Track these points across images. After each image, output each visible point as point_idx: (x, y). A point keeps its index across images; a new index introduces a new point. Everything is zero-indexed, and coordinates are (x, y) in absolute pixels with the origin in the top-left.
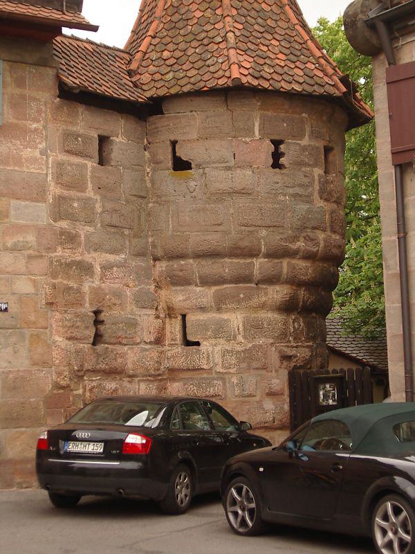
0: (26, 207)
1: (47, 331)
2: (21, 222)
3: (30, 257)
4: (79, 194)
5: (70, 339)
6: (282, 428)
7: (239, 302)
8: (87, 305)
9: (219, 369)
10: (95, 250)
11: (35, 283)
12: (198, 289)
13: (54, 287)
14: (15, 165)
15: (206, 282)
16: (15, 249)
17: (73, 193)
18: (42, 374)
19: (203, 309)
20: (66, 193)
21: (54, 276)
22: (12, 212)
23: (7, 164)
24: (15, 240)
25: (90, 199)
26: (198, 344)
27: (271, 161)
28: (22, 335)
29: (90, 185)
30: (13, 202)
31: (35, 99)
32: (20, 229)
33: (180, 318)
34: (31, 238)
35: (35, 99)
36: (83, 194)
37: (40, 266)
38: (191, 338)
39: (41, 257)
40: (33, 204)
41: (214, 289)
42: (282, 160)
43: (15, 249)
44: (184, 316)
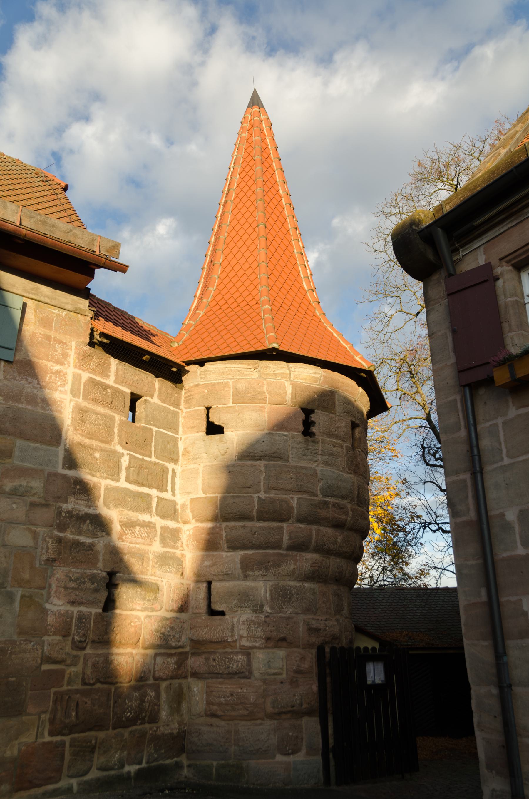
0: (36, 449)
1: (44, 592)
2: (27, 465)
3: (33, 505)
4: (103, 445)
5: (73, 603)
6: (309, 713)
7: (267, 569)
8: (100, 565)
9: (245, 643)
10: (116, 506)
11: (35, 536)
12: (224, 554)
13: (60, 540)
14: (28, 403)
15: (233, 546)
16: (14, 493)
17: (95, 443)
18: (30, 646)
19: (228, 576)
20: (87, 441)
21: (62, 528)
22: (17, 453)
23: (19, 401)
24: (16, 483)
25: (115, 452)
26: (222, 613)
27: (301, 428)
28: (10, 597)
29: (116, 439)
30: (19, 443)
31: (60, 342)
32: (24, 472)
33: (205, 585)
34: (37, 484)
35: (60, 342)
36: (107, 446)
37: (46, 515)
38: (216, 607)
39: (47, 505)
40: (44, 447)
41: (242, 552)
42: (314, 429)
43: (14, 493)
44: (209, 583)
